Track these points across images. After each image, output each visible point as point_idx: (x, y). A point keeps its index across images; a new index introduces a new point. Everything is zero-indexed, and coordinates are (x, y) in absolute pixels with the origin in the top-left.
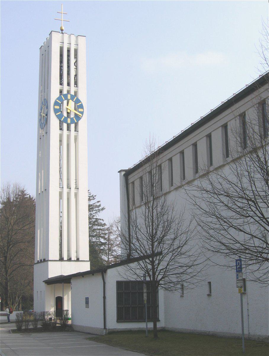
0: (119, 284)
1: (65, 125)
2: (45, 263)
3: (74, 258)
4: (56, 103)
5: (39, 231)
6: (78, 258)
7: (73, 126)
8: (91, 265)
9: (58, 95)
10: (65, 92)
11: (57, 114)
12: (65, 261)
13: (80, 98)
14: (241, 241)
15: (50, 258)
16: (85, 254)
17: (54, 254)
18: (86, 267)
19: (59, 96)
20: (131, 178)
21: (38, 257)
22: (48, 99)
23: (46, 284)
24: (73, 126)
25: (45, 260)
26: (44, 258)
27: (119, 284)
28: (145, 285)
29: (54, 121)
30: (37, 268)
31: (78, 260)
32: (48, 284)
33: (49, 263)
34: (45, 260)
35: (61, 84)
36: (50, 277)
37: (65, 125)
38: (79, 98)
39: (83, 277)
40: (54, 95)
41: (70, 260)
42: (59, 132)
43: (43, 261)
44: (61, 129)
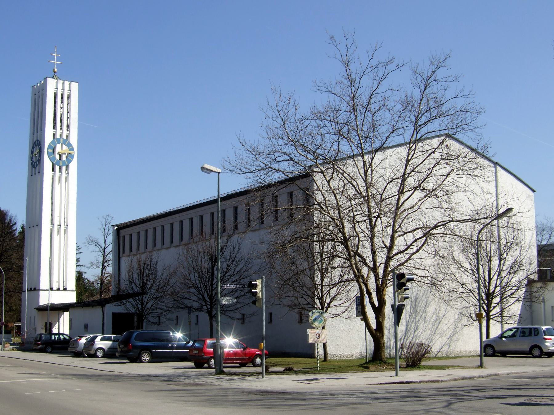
0: (114, 315)
1: (57, 168)
2: (36, 292)
3: (62, 288)
4: (49, 147)
5: (451, 398)
6: (52, 287)
7: (64, 168)
8: (78, 298)
9: (71, 165)
10: (58, 136)
11: (50, 157)
12: (61, 290)
13: (71, 142)
14: (426, 120)
15: (41, 289)
16: (72, 284)
17: (44, 284)
18: (71, 298)
19: (70, 165)
20: (122, 232)
21: (26, 286)
22: (41, 139)
23: (38, 311)
24: (64, 168)
25: (35, 289)
26: (35, 287)
27: (114, 315)
28: (136, 317)
29: (47, 164)
30: (26, 295)
31: (65, 289)
32: (39, 311)
33: (40, 291)
34: (35, 289)
35: (54, 128)
36: (41, 304)
37: (57, 168)
38: (70, 142)
39: (93, 307)
40: (48, 139)
41: (59, 289)
42: (51, 173)
43: (33, 289)
44: (53, 170)
